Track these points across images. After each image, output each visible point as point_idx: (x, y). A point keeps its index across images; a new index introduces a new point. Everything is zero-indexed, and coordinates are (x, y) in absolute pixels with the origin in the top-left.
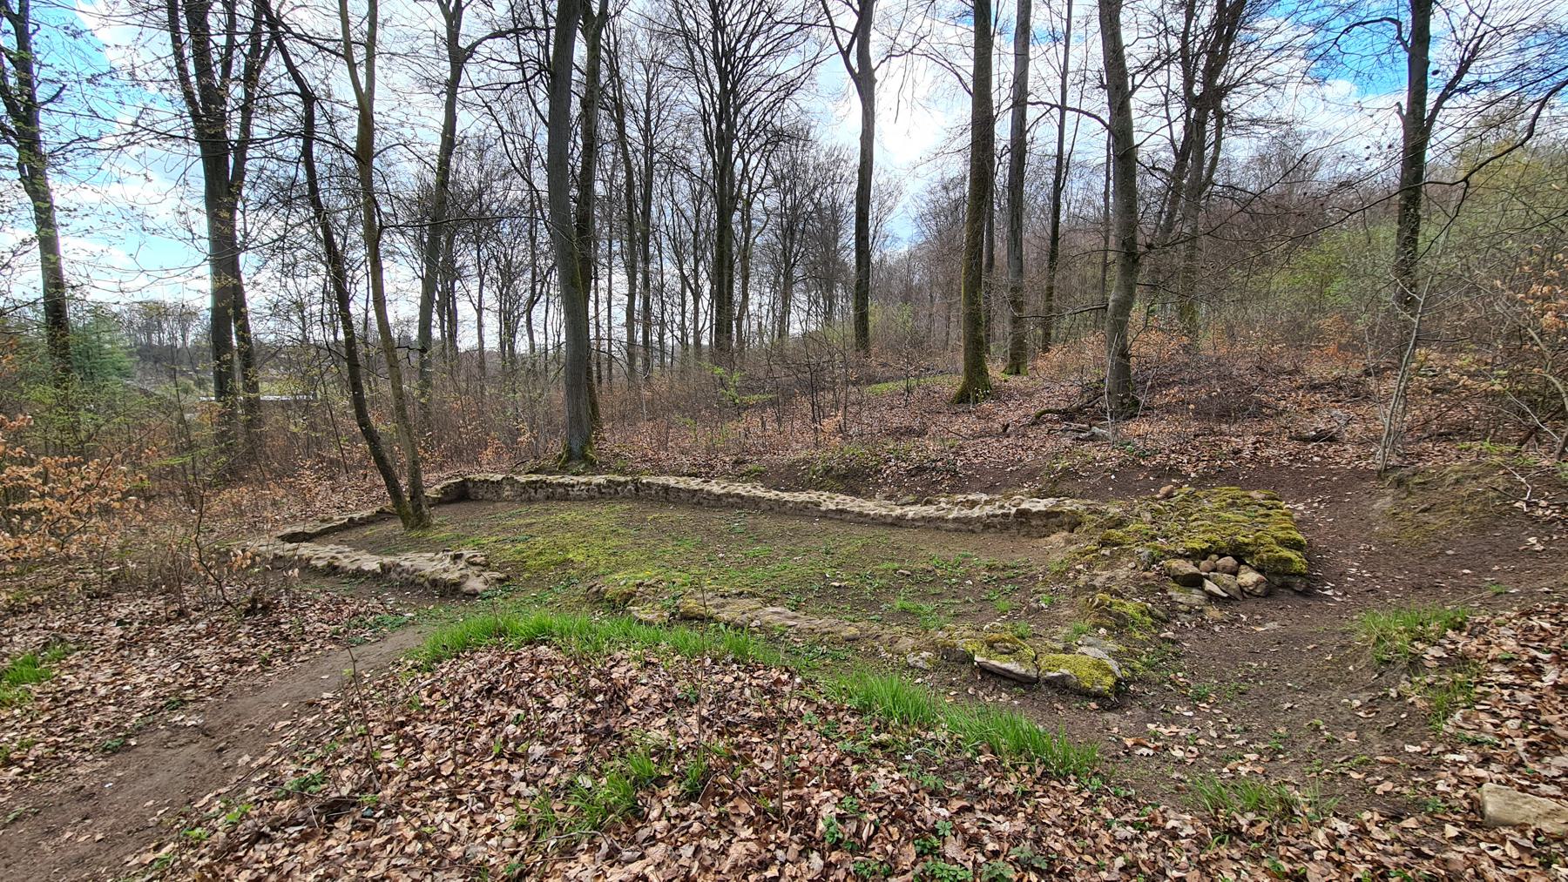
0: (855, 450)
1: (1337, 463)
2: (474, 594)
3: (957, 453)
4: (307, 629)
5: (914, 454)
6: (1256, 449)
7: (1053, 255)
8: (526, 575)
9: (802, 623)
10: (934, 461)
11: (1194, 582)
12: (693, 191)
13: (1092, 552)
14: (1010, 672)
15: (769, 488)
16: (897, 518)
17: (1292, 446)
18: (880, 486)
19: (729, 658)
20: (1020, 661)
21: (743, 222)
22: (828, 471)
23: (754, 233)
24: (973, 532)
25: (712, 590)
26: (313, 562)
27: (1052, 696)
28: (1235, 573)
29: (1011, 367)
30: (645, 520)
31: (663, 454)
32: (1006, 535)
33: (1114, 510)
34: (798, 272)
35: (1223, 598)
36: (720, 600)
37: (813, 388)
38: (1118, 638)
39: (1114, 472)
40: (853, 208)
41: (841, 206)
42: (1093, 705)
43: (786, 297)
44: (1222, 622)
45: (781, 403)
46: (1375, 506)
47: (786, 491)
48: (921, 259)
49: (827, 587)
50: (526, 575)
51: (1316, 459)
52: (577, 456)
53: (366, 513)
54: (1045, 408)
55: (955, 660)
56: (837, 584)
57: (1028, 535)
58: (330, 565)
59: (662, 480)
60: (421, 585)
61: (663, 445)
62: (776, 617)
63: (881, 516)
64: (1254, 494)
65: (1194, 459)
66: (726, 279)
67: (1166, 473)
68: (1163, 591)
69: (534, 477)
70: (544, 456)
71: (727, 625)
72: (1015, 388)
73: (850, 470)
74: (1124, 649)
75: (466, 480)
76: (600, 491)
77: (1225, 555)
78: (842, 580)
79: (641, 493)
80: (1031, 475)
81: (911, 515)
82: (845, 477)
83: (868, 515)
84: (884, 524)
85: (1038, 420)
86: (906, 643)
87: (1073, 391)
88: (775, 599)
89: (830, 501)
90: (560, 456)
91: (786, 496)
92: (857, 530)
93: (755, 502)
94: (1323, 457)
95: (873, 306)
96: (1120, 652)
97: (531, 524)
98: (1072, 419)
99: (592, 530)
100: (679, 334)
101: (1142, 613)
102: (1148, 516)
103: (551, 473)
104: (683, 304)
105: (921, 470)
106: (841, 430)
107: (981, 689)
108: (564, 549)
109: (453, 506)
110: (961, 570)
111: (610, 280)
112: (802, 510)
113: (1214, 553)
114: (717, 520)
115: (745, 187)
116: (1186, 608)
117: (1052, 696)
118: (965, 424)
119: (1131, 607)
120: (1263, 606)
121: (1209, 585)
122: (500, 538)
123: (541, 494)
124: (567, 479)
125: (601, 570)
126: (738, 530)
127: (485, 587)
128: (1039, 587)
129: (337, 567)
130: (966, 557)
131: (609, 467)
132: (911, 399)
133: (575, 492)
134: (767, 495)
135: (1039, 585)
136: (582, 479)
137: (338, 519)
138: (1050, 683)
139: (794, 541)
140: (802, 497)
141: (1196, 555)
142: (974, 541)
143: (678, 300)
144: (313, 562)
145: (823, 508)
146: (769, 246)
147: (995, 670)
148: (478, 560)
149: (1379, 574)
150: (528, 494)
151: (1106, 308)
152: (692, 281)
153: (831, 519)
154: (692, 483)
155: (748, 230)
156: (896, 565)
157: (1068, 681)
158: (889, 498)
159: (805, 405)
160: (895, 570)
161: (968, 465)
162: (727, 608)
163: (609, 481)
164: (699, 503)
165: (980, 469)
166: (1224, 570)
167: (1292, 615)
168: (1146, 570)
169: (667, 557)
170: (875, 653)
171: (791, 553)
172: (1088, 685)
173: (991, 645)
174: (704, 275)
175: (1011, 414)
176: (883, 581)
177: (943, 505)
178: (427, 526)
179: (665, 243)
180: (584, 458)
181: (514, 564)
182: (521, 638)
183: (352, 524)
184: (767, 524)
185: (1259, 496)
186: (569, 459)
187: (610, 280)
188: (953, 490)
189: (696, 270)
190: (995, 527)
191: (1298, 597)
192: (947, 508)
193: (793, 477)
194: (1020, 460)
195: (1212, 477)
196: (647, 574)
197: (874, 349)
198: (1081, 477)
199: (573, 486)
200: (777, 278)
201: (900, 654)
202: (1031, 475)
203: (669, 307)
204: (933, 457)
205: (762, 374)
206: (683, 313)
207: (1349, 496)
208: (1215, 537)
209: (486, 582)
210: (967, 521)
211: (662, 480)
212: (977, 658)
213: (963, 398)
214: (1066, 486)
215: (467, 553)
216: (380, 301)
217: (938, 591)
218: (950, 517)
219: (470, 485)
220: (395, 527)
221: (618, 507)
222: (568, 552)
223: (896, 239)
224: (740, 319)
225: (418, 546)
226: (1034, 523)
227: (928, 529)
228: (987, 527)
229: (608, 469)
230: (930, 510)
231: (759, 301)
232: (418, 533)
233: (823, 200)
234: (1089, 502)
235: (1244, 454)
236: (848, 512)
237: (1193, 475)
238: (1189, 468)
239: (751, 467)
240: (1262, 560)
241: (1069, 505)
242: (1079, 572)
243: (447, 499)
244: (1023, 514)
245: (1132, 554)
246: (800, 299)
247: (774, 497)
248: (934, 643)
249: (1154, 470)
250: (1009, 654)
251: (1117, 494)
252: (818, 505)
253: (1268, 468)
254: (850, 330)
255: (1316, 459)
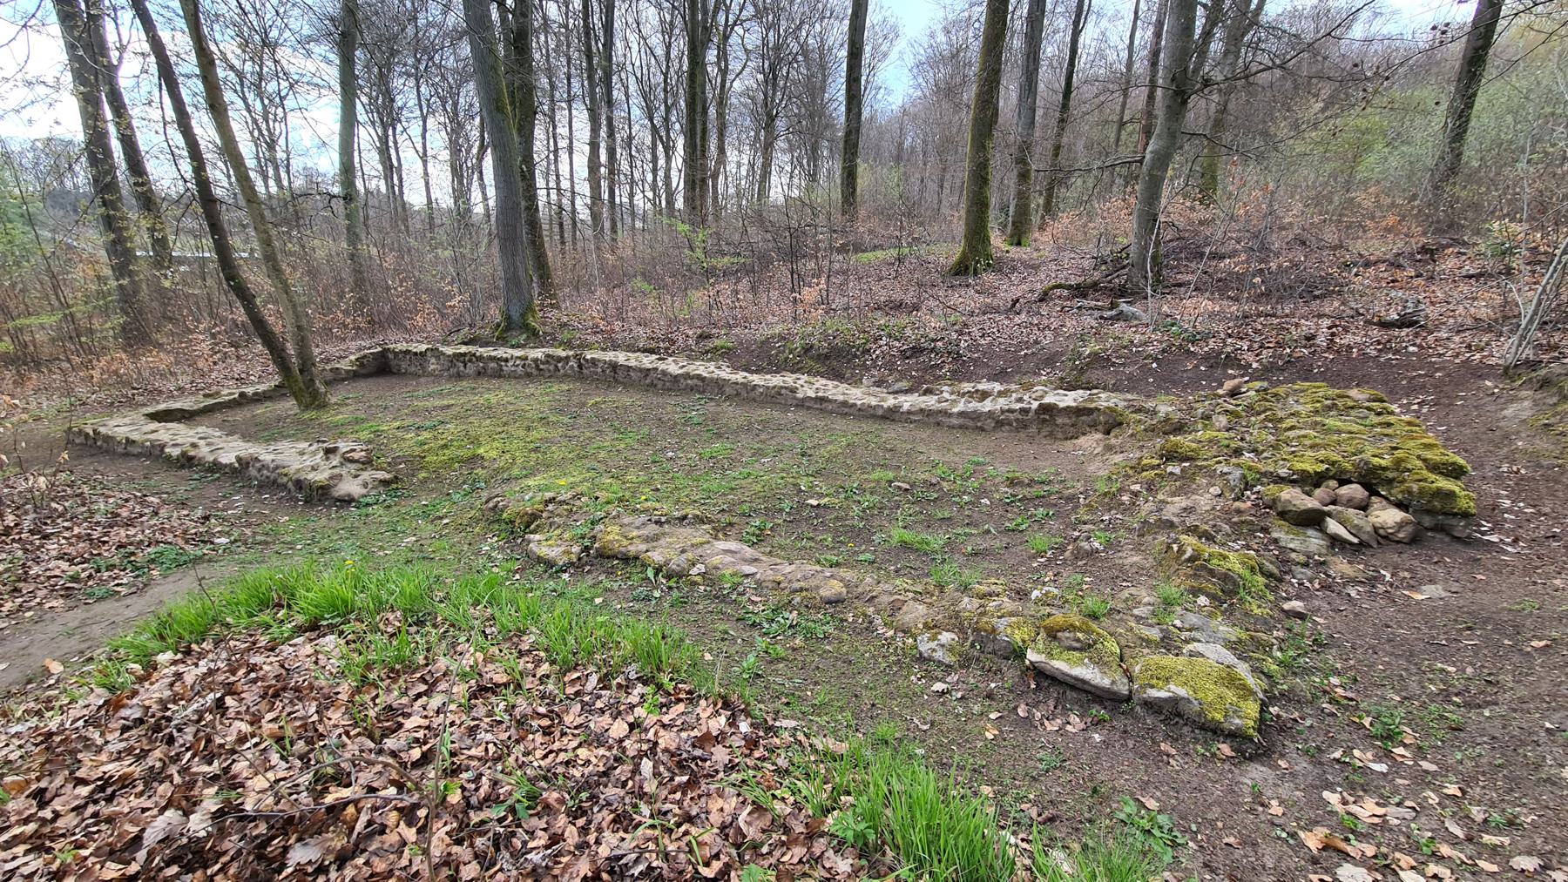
0: (840, 325)
1: (1440, 355)
2: (347, 501)
3: (960, 333)
4: (35, 570)
5: (908, 332)
6: (1333, 334)
7: (1065, 106)
8: (423, 475)
9: (763, 571)
10: (934, 340)
11: (1313, 520)
12: (662, 22)
13: (1153, 468)
14: (1084, 681)
15: (736, 368)
16: (889, 409)
17: (1375, 332)
18: (868, 369)
19: (632, 671)
20: (1100, 662)
21: (718, 63)
22: (807, 349)
23: (731, 77)
24: (982, 429)
25: (645, 511)
26: (167, 450)
27: (1154, 729)
28: (1364, 507)
29: (1012, 236)
30: (584, 404)
31: (617, 325)
32: (1022, 435)
33: (1165, 407)
34: (781, 124)
35: (1351, 544)
36: (652, 529)
37: (793, 254)
38: (1229, 613)
39: (1156, 360)
40: (844, 53)
41: (830, 49)
42: (1226, 749)
43: (768, 148)
44: (1354, 581)
45: (755, 269)
46: (1505, 412)
47: (757, 372)
48: (915, 117)
49: (803, 505)
50: (423, 475)
51: (1411, 349)
52: (514, 327)
53: (261, 388)
54: (1053, 282)
55: (994, 652)
56: (814, 502)
57: (1051, 435)
58: (184, 454)
59: (610, 356)
60: (285, 486)
61: (620, 315)
62: (728, 559)
63: (870, 406)
64: (1354, 393)
65: (1256, 346)
66: (699, 128)
67: (1222, 362)
68: (1265, 530)
69: (464, 349)
70: (479, 324)
71: (657, 571)
72: (1019, 260)
73: (833, 348)
74: (1244, 636)
75: (386, 351)
76: (537, 366)
77: (1349, 482)
78: (821, 496)
79: (585, 372)
80: (1050, 361)
81: (906, 407)
82: (827, 357)
83: (855, 405)
84: (874, 416)
85: (1044, 298)
86: (915, 613)
87: (1086, 263)
88: (731, 524)
89: (809, 386)
90: (498, 325)
91: (756, 379)
92: (840, 424)
93: (719, 385)
94: (1420, 347)
95: (862, 168)
96: (1240, 641)
97: (449, 406)
98: (1085, 296)
99: (517, 416)
100: (650, 195)
101: (1252, 569)
102: (1223, 420)
103: (486, 344)
104: (655, 159)
105: (917, 351)
106: (824, 301)
107: (1036, 705)
108: (476, 442)
109: (370, 380)
110: (973, 483)
111: (570, 127)
112: (775, 397)
113: (1333, 478)
114: (671, 406)
115: (721, 18)
116: (1302, 559)
117: (1154, 729)
118: (966, 299)
119: (1234, 560)
120: (1407, 558)
121: (1333, 526)
122: (406, 423)
123: (471, 369)
124: (501, 352)
125: (516, 472)
126: (696, 420)
127: (364, 491)
128: (1082, 514)
129: (192, 458)
130: (978, 464)
131: (554, 339)
132: (903, 270)
133: (510, 366)
134: (733, 377)
135: (1082, 511)
136: (518, 353)
137: (229, 392)
138: (1152, 706)
139: (763, 437)
140: (775, 380)
141: (1309, 481)
142: (984, 442)
143: (649, 157)
144: (167, 450)
145: (800, 396)
146: (747, 92)
147: (1060, 677)
148: (356, 456)
149: (1547, 510)
150: (458, 368)
151: (1141, 162)
152: (663, 134)
153: (809, 408)
154: (645, 360)
155: (724, 72)
156: (891, 475)
157: (1182, 707)
158: (879, 384)
159: (783, 274)
160: (890, 482)
161: (974, 347)
162: (662, 542)
163: (548, 356)
164: (652, 385)
165: (988, 352)
166: (1350, 503)
167: (1455, 572)
168: (1237, 499)
169: (602, 455)
170: (870, 627)
171: (759, 453)
172: (1219, 717)
173: (1052, 634)
174: (677, 126)
175: (1010, 289)
176: (876, 498)
177: (946, 395)
178: (323, 406)
179: (633, 88)
180: (526, 327)
181: (408, 460)
182: (300, 619)
183: (243, 401)
184: (732, 414)
185: (1361, 397)
186: (508, 329)
187: (570, 127)
188: (957, 376)
189: (666, 119)
190: (1010, 424)
191: (1459, 547)
192: (950, 399)
193: (765, 357)
194: (1036, 342)
195: (1279, 369)
196: (563, 484)
197: (862, 213)
198: (1113, 364)
199: (506, 360)
200: (757, 134)
201: (906, 632)
202: (1050, 361)
203: (639, 163)
204: (932, 335)
205: (737, 237)
206: (655, 171)
207: (1462, 398)
208: (1336, 457)
209: (365, 485)
210: (975, 416)
211: (610, 356)
212: (1032, 656)
213: (962, 269)
214: (1094, 375)
215: (343, 446)
216: (390, 169)
217: (947, 515)
218: (955, 410)
219: (391, 356)
220: (289, 405)
221: (555, 388)
222: (480, 445)
223: (889, 92)
224: (715, 177)
225: (301, 430)
226: (1059, 421)
227: (927, 425)
228: (1000, 424)
229: (555, 341)
230: (930, 402)
231: (738, 161)
232: (313, 414)
233: (811, 41)
234: (1129, 396)
235: (1318, 341)
236: (830, 401)
237: (1255, 365)
238: (1250, 357)
239: (717, 342)
240: (1410, 492)
241: (1105, 400)
242: (1136, 494)
243: (363, 371)
244: (1047, 409)
245: (1211, 474)
246: (781, 159)
247: (741, 380)
248: (957, 615)
249: (1206, 358)
250: (1080, 650)
251: (1159, 387)
252: (793, 390)
253: (1349, 359)
254: (837, 195)
255: (1411, 349)
